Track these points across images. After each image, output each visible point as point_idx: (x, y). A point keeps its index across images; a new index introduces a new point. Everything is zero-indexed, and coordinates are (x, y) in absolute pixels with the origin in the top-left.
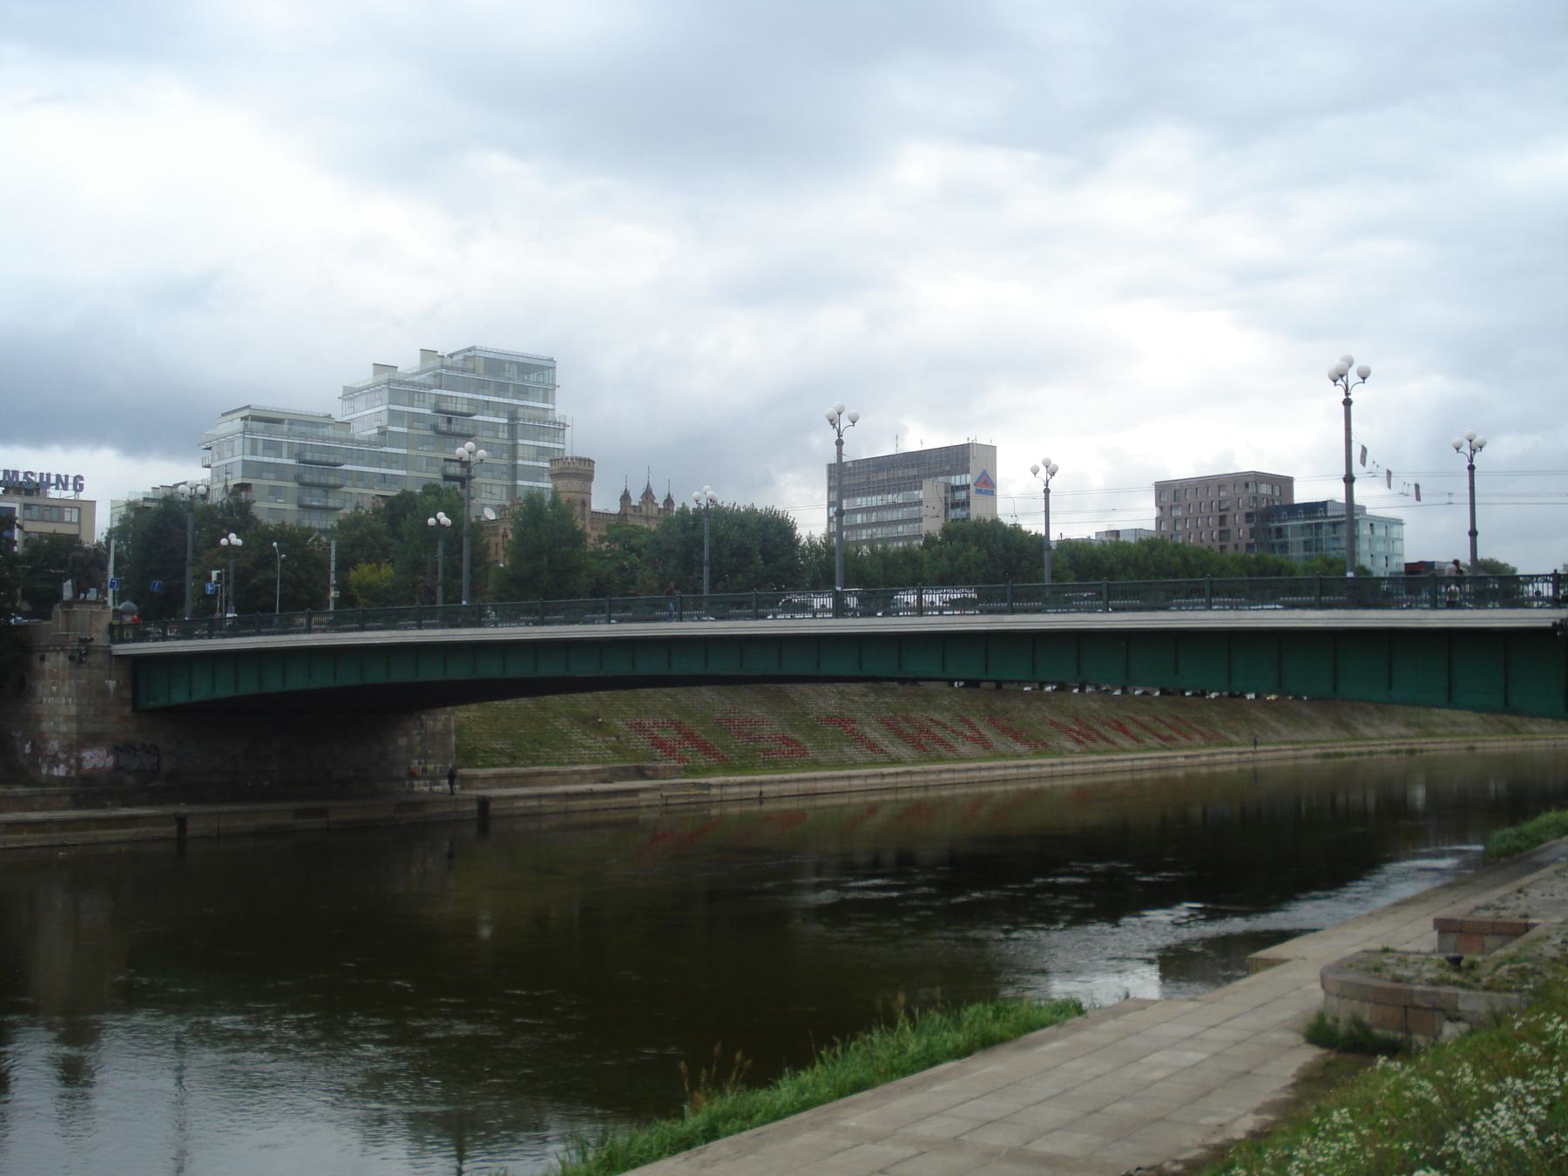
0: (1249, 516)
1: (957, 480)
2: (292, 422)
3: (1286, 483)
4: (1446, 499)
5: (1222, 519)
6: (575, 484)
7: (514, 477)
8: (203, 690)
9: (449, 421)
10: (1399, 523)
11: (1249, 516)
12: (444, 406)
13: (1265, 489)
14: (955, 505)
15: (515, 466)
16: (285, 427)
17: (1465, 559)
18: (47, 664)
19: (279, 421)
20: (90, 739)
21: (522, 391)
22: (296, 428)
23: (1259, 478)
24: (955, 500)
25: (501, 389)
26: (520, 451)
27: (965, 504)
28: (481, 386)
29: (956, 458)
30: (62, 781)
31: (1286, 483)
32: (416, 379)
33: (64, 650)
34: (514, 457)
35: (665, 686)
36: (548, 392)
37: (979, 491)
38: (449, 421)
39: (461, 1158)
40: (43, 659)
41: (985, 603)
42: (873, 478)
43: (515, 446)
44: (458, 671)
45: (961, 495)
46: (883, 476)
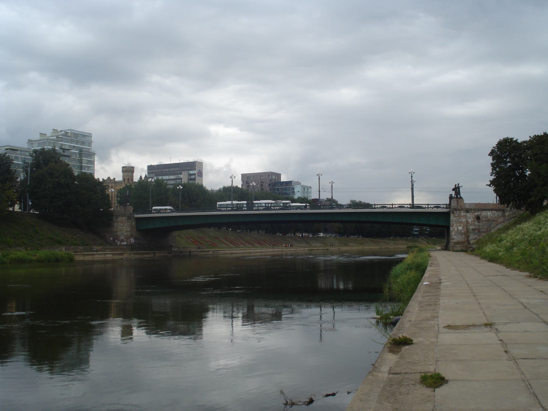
0: (270, 184)
1: (191, 172)
2: (21, 151)
3: (279, 175)
4: (429, 206)
5: (262, 185)
6: (130, 174)
7: (81, 169)
8: (151, 226)
9: (64, 152)
10: (311, 188)
11: (270, 184)
12: (63, 147)
13: (274, 177)
14: (191, 179)
15: (81, 166)
16: (19, 152)
17: (330, 197)
18: (119, 219)
19: (17, 150)
20: (131, 236)
21: (83, 143)
22: (23, 153)
23: (272, 174)
24: (191, 178)
25: (77, 142)
26: (83, 161)
27: (195, 179)
28: (72, 141)
29: (191, 166)
30: (126, 245)
31: (279, 175)
32: (51, 138)
33: (125, 216)
34: (81, 163)
35: (182, 229)
36: (90, 144)
37: (198, 176)
38: (64, 152)
39: (233, 307)
40: (117, 218)
41: (177, 209)
42: (163, 170)
43: (82, 160)
44: (188, 223)
45: (193, 177)
46: (167, 170)
